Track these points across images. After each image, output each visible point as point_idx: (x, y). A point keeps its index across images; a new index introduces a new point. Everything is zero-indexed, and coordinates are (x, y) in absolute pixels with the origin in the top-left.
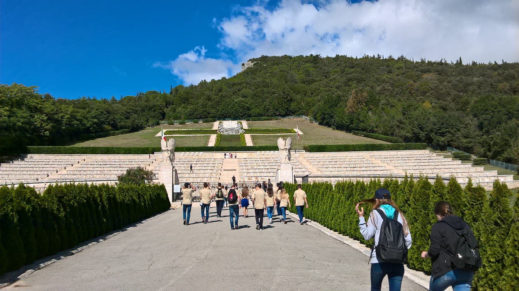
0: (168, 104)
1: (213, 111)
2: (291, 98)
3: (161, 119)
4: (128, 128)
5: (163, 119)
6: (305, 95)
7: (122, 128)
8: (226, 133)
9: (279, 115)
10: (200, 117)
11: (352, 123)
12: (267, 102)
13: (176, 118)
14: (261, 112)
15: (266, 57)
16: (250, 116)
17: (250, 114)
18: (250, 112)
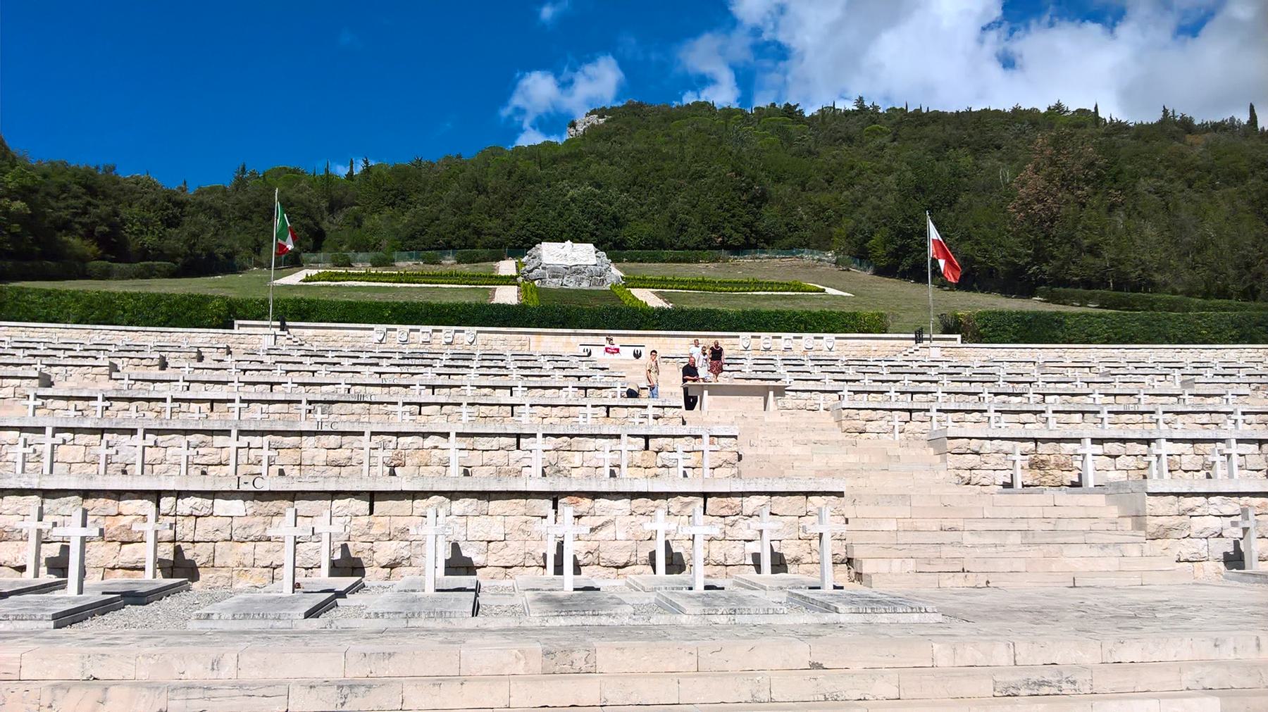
0: (335, 206)
1: (494, 224)
2: (763, 194)
3: (307, 250)
4: (172, 258)
5: (317, 248)
6: (803, 185)
7: (144, 255)
8: (553, 284)
9: (724, 246)
10: (448, 243)
11: (1040, 257)
13: (362, 246)
14: (662, 234)
17: (623, 241)
18: (624, 233)
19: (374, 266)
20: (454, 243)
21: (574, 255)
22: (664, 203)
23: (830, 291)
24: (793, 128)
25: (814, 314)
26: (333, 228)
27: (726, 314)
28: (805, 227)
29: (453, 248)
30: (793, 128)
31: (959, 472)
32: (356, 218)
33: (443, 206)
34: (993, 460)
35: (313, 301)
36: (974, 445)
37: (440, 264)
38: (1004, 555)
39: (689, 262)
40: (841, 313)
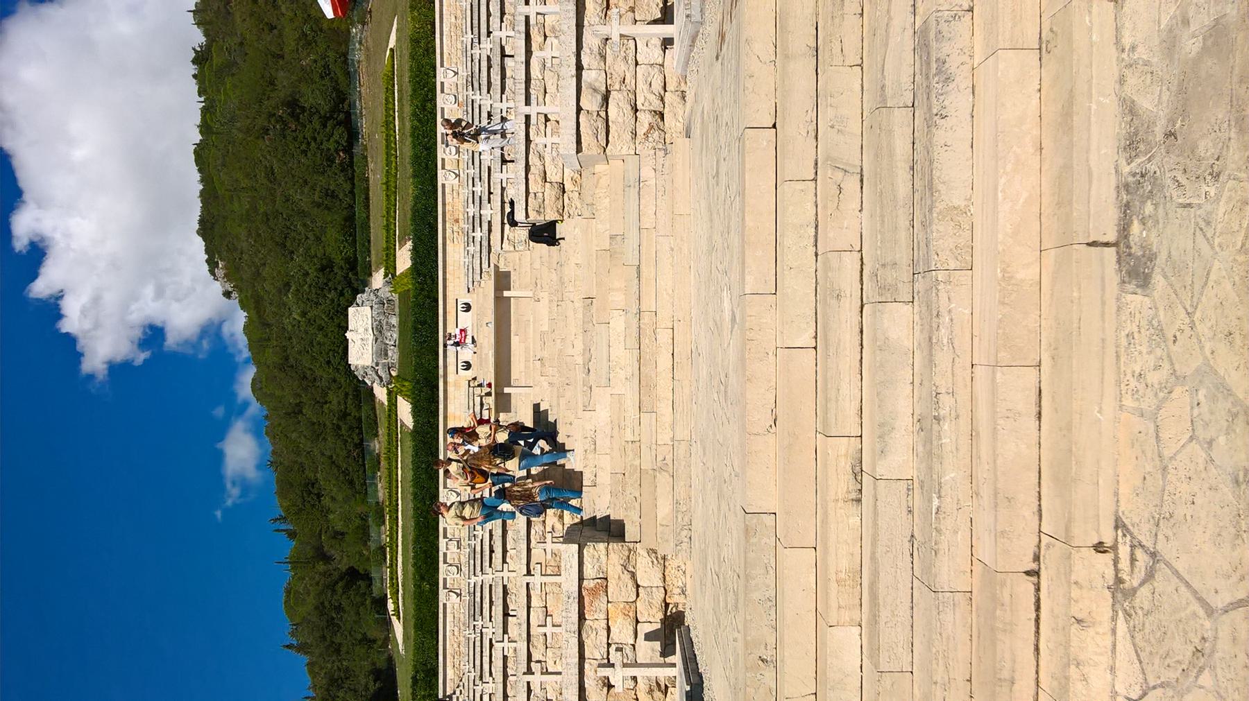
5: (368, 578)
8: (394, 355)
9: (349, 149)
10: (356, 446)
12: (302, 199)
13: (364, 534)
15: (201, 222)
16: (352, 264)
17: (347, 260)
18: (338, 259)
19: (384, 523)
20: (357, 440)
21: (361, 330)
22: (303, 214)
23: (392, 43)
24: (217, 60)
25: (414, 90)
26: (345, 559)
27: (416, 198)
28: (324, 57)
29: (362, 440)
30: (217, 60)
31: (641, 131)
32: (334, 538)
33: (316, 452)
34: (619, 68)
35: (415, 666)
36: (591, 103)
37: (378, 455)
38: (963, 395)
39: (368, 189)
40: (412, 57)
